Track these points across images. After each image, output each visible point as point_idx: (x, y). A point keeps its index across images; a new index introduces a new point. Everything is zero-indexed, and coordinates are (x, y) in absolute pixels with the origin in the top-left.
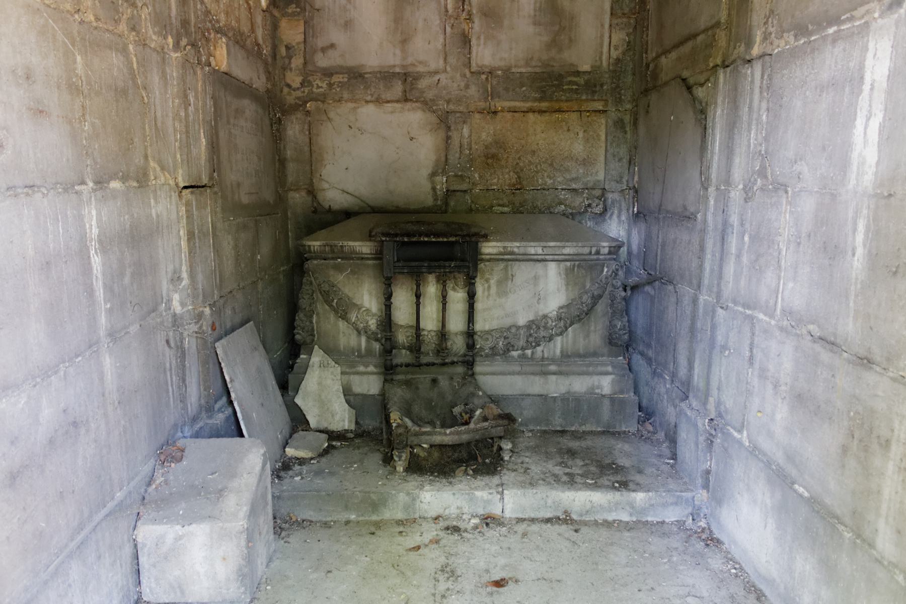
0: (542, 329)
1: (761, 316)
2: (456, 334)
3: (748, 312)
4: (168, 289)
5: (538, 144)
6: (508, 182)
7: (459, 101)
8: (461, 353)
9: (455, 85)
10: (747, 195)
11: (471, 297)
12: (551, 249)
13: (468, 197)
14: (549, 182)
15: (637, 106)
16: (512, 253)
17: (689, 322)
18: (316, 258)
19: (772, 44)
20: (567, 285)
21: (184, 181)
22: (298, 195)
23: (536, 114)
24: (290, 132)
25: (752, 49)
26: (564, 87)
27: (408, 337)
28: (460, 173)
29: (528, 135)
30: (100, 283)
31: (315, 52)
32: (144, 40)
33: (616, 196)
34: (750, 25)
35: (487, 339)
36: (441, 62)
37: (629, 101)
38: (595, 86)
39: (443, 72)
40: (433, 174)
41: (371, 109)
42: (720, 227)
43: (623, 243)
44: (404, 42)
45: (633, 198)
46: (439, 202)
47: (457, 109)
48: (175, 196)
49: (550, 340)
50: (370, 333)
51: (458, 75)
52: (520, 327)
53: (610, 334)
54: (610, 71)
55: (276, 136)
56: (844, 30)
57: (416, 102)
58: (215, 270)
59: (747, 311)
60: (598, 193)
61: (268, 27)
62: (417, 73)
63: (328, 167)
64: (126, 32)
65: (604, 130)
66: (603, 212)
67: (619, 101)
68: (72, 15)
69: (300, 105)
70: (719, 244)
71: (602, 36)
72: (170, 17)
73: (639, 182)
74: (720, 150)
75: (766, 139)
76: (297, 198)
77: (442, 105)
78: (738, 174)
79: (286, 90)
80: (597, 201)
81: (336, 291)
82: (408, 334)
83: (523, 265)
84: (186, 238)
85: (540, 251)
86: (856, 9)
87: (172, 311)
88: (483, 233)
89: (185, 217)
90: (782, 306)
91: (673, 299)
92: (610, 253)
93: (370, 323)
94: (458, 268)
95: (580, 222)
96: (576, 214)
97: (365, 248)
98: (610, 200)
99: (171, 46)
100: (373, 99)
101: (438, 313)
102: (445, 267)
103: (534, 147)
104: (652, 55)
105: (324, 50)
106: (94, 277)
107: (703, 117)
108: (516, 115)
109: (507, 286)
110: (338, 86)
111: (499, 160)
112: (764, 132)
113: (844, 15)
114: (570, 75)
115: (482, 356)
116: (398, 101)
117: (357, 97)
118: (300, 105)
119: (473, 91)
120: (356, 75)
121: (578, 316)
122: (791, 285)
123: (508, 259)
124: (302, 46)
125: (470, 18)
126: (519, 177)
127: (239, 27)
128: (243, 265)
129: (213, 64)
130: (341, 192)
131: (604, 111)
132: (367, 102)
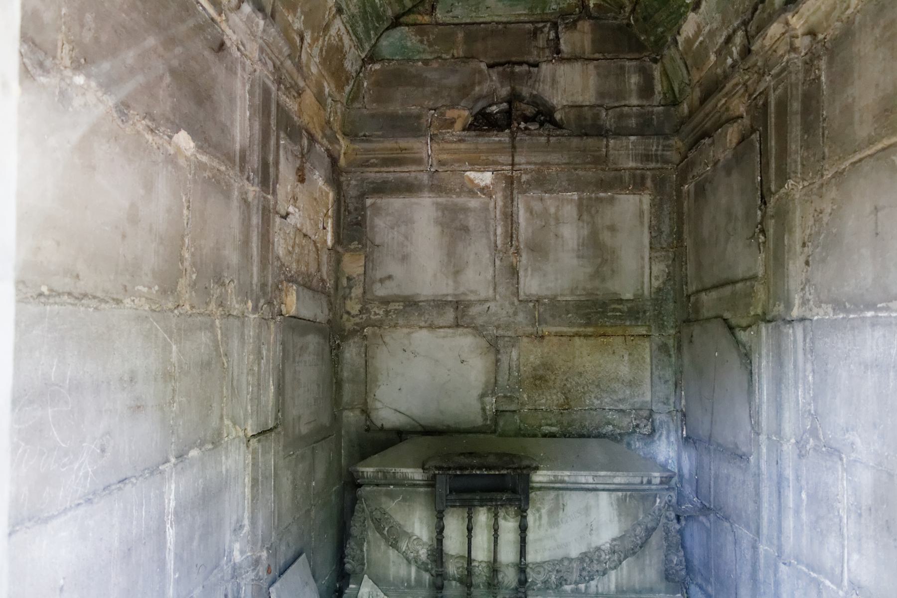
0: (595, 562)
1: (828, 583)
2: (508, 565)
3: (814, 575)
4: (231, 541)
5: (584, 366)
6: (556, 402)
7: (508, 326)
8: (512, 587)
9: (505, 312)
10: (800, 451)
11: (523, 529)
12: (601, 478)
13: (516, 417)
14: (597, 402)
15: (679, 332)
16: (563, 482)
17: (749, 567)
18: (369, 485)
19: (811, 310)
20: (620, 515)
21: (253, 431)
22: (352, 414)
23: (582, 338)
24: (347, 355)
25: (792, 310)
26: (609, 314)
27: (458, 568)
28: (509, 394)
29: (574, 358)
30: (172, 554)
31: (373, 282)
32: (228, 311)
33: (664, 417)
34: (788, 290)
35: (539, 573)
36: (491, 292)
37: (672, 327)
38: (638, 313)
39: (493, 300)
40: (483, 396)
41: (424, 333)
42: (775, 477)
43: (675, 474)
44: (457, 273)
45: (682, 421)
46: (489, 422)
47: (506, 334)
48: (243, 447)
49: (604, 574)
50: (420, 563)
51: (507, 303)
52: (572, 559)
53: (666, 570)
54: (652, 299)
55: (334, 361)
56: (881, 317)
57: (467, 327)
58: (274, 511)
59: (812, 573)
60: (645, 413)
61: (333, 263)
62: (468, 301)
63: (382, 387)
64: (214, 310)
65: (649, 353)
66: (651, 433)
67: (662, 327)
68: (172, 312)
69: (359, 330)
70: (775, 495)
71: (643, 267)
72: (251, 284)
73: (686, 406)
74: (768, 400)
75: (815, 399)
76: (352, 417)
77: (492, 330)
78: (788, 428)
79: (345, 316)
80: (645, 421)
81: (387, 519)
82: (459, 565)
83: (575, 495)
84: (250, 485)
85: (591, 480)
86: (892, 301)
87: (232, 563)
88: (534, 465)
89: (250, 464)
90: (849, 577)
91: (730, 538)
92: (661, 483)
93: (421, 552)
94: (510, 502)
95: (629, 444)
96: (624, 434)
97: (416, 474)
98: (658, 421)
99: (250, 309)
100: (426, 325)
101: (489, 542)
102: (496, 500)
103: (581, 369)
104: (692, 288)
105: (381, 281)
106: (168, 550)
107: (748, 361)
108: (563, 339)
109: (558, 515)
110: (394, 313)
111: (546, 381)
112: (811, 392)
113: (881, 303)
114: (614, 303)
115: (534, 590)
116: (449, 327)
117: (412, 323)
118: (359, 330)
119: (521, 317)
120: (411, 304)
121: (633, 549)
122: (855, 557)
123: (560, 488)
124: (362, 278)
125: (518, 252)
126: (567, 398)
127: (307, 270)
128: (299, 497)
129: (284, 312)
130: (393, 411)
131: (648, 336)
132: (421, 328)
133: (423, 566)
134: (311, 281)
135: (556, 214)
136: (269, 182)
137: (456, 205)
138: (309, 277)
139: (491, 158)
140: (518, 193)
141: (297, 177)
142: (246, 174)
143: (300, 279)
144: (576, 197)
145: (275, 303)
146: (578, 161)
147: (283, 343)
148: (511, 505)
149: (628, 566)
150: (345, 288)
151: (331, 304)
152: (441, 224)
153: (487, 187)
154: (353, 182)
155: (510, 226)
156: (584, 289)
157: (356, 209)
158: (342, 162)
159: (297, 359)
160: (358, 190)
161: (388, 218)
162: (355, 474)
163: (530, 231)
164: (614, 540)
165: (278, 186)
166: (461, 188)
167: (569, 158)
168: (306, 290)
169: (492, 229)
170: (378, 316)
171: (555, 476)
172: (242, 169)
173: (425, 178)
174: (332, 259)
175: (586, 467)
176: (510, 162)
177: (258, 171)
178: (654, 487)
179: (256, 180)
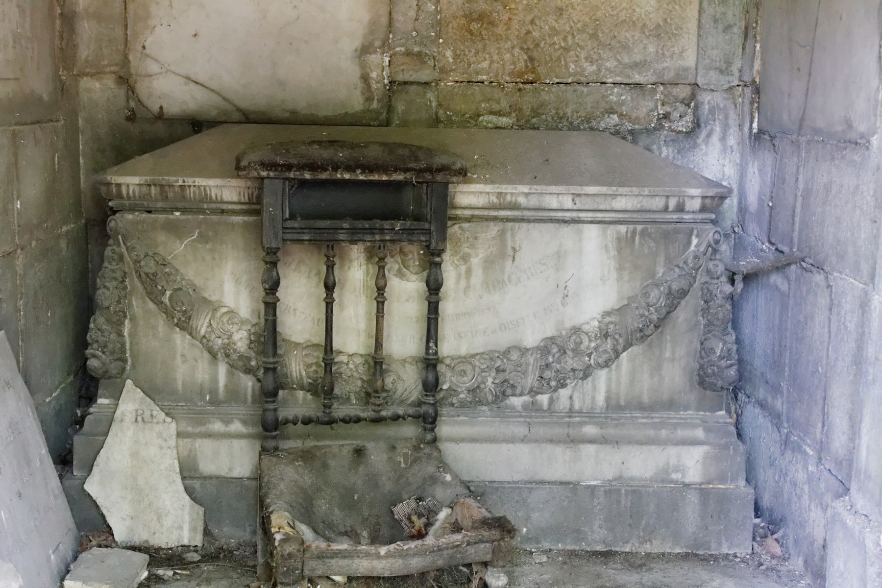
0: (570, 353)
2: (405, 361)
6: (509, 67)
11: (434, 288)
12: (589, 200)
13: (430, 95)
14: (590, 69)
16: (515, 207)
17: (853, 344)
18: (132, 209)
20: (620, 269)
22: (98, 85)
27: (309, 366)
28: (416, 49)
33: (718, 99)
35: (464, 373)
40: (365, 50)
43: (730, 191)
45: (752, 103)
46: (375, 105)
49: (585, 377)
50: (235, 356)
52: (527, 350)
53: (702, 367)
60: (683, 92)
63: (158, 29)
73: (763, 73)
80: (681, 108)
82: (310, 360)
83: (536, 230)
85: (568, 203)
88: (458, 166)
92: (703, 209)
93: (236, 337)
96: (641, 132)
98: (707, 107)
101: (369, 320)
102: (382, 231)
111: (492, 24)
115: (452, 405)
121: (641, 331)
126: (531, 59)
130: (183, 80)
133: (240, 363)
148: (410, 242)
149: (631, 360)
162: (103, 189)
164: (608, 314)
171: (499, 195)
175: (561, 179)
178: (686, 217)
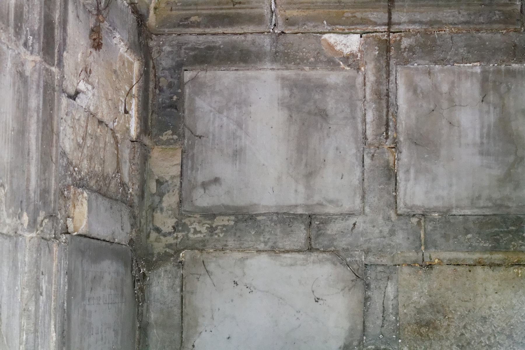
7: (381, 251)
23: (486, 269)
31: (194, 187)
41: (264, 258)
44: (310, 175)
47: (379, 262)
51: (380, 218)
55: (138, 297)
57: (324, 251)
62: (326, 214)
63: (204, 334)
72: (28, 190)
77: (360, 257)
79: (154, 235)
100: (267, 248)
103: (485, 312)
105: (205, 185)
108: (459, 268)
111: (436, 328)
116: (299, 251)
117: (246, 245)
119: (400, 238)
124: (177, 181)
125: (395, 146)
127: (103, 170)
129: (71, 229)
132: (259, 251)
134: (108, 186)
135: (450, 92)
136: (54, 49)
137: (308, 80)
138: (105, 179)
139: (359, 15)
140: (396, 64)
141: (90, 42)
142: (23, 37)
143: (92, 183)
144: (478, 70)
145: (59, 216)
146: (481, 19)
147: (69, 273)
150: (153, 195)
151: (135, 217)
152: (289, 108)
153: (353, 55)
154: (167, 48)
155: (385, 110)
156: (490, 199)
157: (170, 86)
158: (152, 20)
159: (88, 294)
160: (172, 59)
161: (217, 98)
163: (413, 116)
165: (65, 54)
166: (316, 58)
167: (469, 14)
168: (100, 198)
169: (359, 114)
170: (199, 235)
172: (18, 33)
173: (266, 42)
174: (137, 156)
176: (386, 21)
177: (39, 34)
179: (36, 46)
